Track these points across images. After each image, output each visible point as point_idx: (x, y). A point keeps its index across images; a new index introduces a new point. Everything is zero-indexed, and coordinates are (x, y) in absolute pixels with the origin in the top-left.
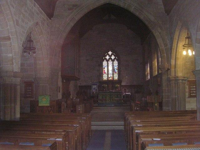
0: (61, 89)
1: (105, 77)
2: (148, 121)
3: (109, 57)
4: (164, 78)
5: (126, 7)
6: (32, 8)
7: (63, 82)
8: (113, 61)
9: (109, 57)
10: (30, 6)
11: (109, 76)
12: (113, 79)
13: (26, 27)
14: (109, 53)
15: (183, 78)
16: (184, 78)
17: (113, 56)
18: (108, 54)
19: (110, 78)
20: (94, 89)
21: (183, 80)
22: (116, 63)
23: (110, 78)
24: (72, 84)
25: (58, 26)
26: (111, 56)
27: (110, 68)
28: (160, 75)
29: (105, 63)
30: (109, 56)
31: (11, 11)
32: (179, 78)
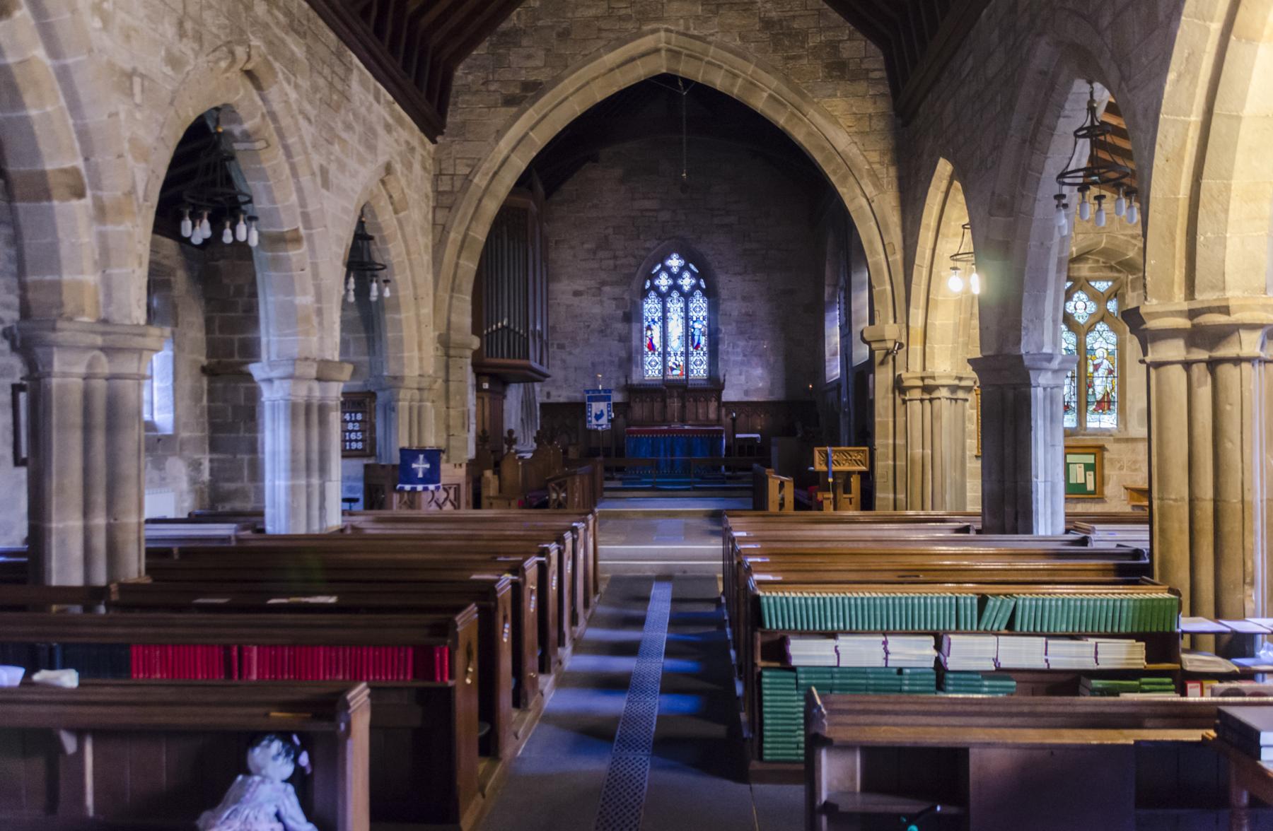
0: (473, 420)
1: (651, 369)
2: (734, 489)
3: (671, 282)
4: (882, 379)
5: (736, 91)
6: (369, 109)
7: (478, 388)
8: (687, 296)
9: (671, 282)
10: (362, 104)
11: (671, 361)
12: (687, 376)
13: (353, 190)
14: (669, 263)
15: (956, 382)
16: (960, 379)
17: (687, 275)
18: (667, 269)
19: (676, 372)
20: (598, 417)
21: (954, 389)
22: (699, 307)
23: (675, 372)
24: (514, 395)
25: (467, 171)
26: (679, 275)
27: (676, 328)
28: (869, 366)
29: (651, 307)
30: (671, 275)
31: (301, 137)
32: (938, 382)
